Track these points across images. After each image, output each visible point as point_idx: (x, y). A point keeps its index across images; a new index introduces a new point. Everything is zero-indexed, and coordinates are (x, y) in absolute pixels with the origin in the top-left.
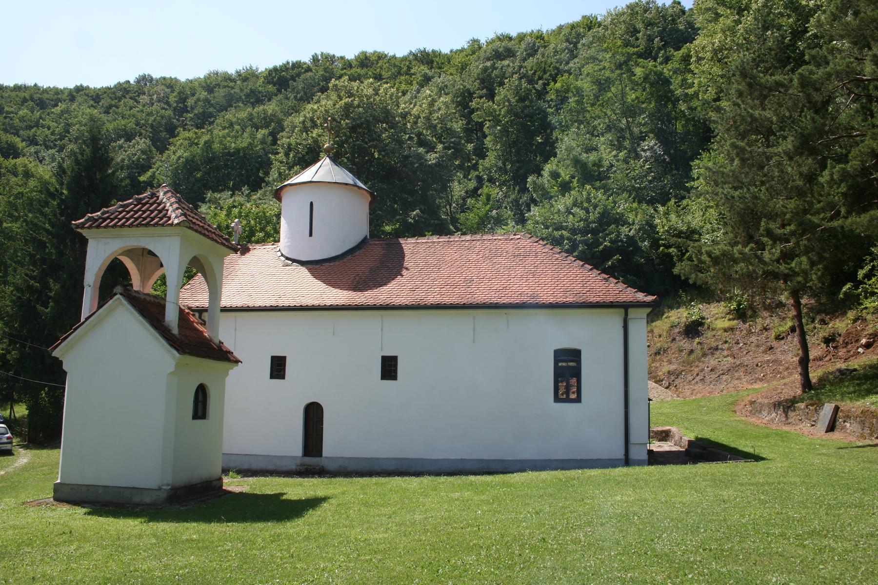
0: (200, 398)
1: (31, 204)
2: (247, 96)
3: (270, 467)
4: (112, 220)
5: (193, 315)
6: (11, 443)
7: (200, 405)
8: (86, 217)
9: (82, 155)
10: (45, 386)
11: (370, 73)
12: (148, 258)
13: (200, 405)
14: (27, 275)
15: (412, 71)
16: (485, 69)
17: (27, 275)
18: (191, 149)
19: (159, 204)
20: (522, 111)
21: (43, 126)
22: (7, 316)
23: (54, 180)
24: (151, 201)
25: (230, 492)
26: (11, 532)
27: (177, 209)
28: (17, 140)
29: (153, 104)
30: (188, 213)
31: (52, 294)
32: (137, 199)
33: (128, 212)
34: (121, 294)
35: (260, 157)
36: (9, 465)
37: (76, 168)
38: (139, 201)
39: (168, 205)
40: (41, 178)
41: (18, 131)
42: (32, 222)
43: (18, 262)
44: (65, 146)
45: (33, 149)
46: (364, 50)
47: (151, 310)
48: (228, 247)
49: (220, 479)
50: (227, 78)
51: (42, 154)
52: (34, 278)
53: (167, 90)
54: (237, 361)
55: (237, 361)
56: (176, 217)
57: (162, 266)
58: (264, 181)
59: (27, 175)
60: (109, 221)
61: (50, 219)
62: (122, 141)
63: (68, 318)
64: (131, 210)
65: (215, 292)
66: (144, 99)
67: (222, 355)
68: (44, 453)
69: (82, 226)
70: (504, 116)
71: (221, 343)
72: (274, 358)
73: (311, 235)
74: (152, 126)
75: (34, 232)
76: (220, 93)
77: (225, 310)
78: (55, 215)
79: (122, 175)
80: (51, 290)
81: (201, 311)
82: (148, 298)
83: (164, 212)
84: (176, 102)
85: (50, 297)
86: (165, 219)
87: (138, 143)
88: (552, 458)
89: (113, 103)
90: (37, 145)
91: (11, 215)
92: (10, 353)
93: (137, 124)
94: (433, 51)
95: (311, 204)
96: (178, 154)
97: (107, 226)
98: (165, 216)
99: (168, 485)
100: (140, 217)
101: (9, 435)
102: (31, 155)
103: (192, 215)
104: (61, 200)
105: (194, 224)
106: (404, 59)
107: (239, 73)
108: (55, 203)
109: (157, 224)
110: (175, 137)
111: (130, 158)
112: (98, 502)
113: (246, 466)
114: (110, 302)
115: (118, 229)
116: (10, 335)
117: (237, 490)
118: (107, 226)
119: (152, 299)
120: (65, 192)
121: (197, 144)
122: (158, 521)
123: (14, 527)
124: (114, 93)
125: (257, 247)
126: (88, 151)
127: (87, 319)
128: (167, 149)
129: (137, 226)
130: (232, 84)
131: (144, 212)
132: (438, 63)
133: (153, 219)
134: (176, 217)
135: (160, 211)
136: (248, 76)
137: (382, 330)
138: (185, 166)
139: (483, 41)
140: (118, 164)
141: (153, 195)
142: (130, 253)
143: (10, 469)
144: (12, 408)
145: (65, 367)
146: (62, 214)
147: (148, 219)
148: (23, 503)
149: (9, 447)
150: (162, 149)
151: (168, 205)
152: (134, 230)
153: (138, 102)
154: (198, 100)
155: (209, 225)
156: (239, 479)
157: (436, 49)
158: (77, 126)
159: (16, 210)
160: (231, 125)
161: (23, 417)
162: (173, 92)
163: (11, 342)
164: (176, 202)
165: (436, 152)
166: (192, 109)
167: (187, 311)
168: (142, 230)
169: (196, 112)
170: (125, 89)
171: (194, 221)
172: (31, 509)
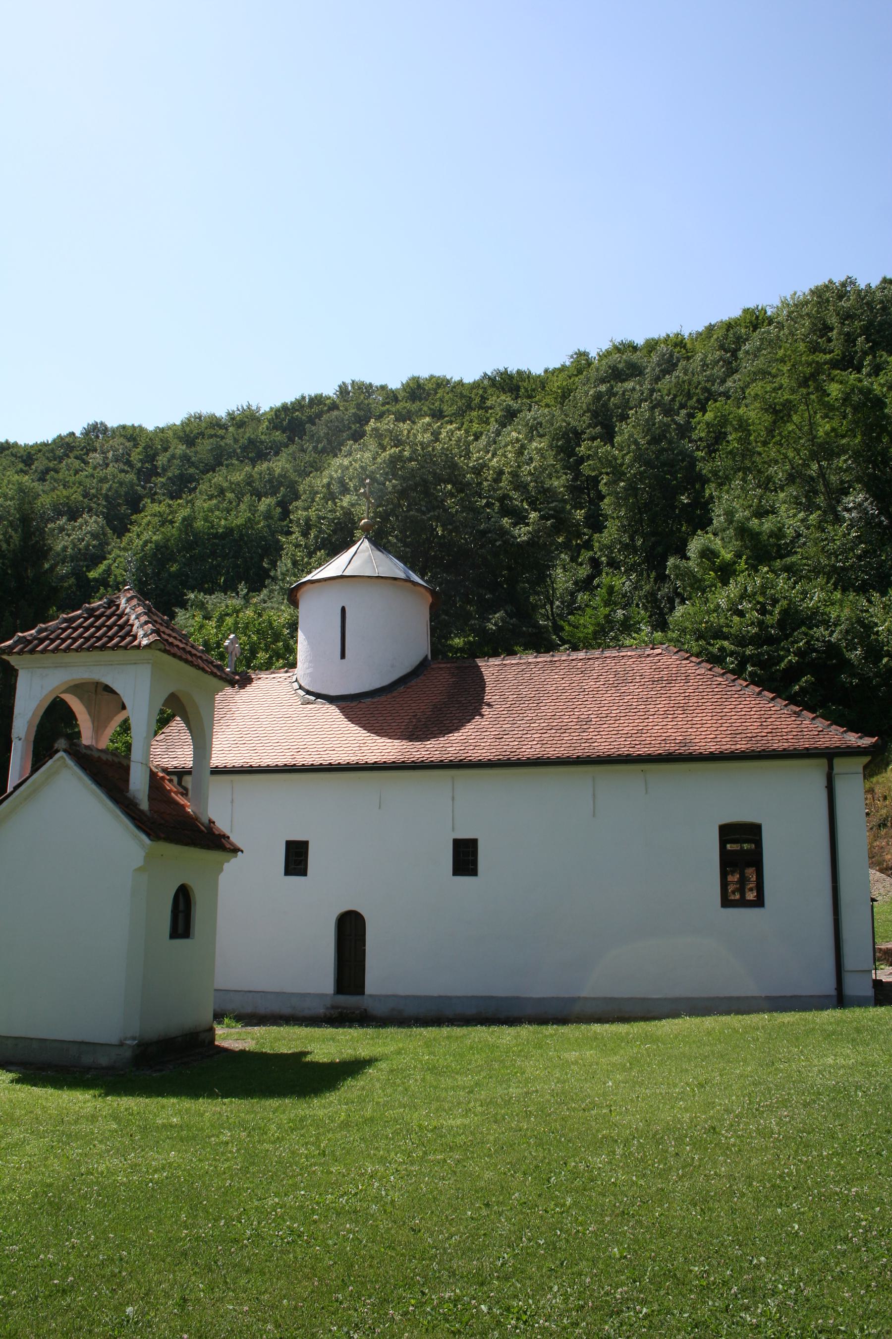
0: (182, 906)
2: (244, 448)
3: (286, 1011)
4: (53, 641)
5: (171, 781)
7: (181, 916)
8: (16, 638)
11: (425, 409)
12: (102, 696)
13: (181, 916)
15: (489, 403)
16: (598, 397)
19: (120, 617)
20: (657, 458)
24: (108, 612)
27: (146, 623)
29: (107, 465)
30: (162, 629)
32: (87, 609)
33: (75, 629)
34: (65, 751)
35: (263, 538)
38: (91, 612)
39: (133, 617)
46: (416, 375)
47: (108, 773)
48: (220, 678)
49: (211, 1030)
50: (214, 423)
53: (128, 444)
54: (235, 850)
55: (235, 850)
56: (145, 635)
57: (124, 707)
58: (269, 577)
64: (80, 626)
66: (95, 458)
67: (214, 842)
69: (9, 650)
70: (631, 466)
71: (211, 822)
72: (289, 844)
73: (343, 656)
74: (106, 497)
76: (204, 446)
81: (181, 774)
82: (104, 757)
83: (127, 628)
84: (141, 460)
86: (129, 639)
88: (721, 995)
89: (51, 465)
93: (86, 495)
94: (519, 372)
95: (343, 610)
98: (128, 634)
99: (134, 1038)
100: (92, 636)
103: (168, 631)
105: (171, 645)
106: (476, 385)
107: (231, 416)
110: (140, 512)
111: (75, 545)
113: (249, 1010)
115: (60, 655)
119: (110, 758)
121: (172, 522)
122: (119, 1095)
124: (52, 451)
126: (16, 537)
127: (16, 788)
128: (129, 531)
129: (88, 649)
130: (221, 432)
131: (98, 629)
132: (526, 390)
133: (111, 639)
134: (145, 635)
135: (121, 627)
136: (244, 420)
137: (232, 802)
138: (155, 554)
139: (593, 354)
142: (78, 689)
147: (105, 639)
150: (121, 530)
151: (133, 617)
152: (84, 654)
153: (86, 463)
154: (173, 457)
155: (193, 646)
156: (238, 1029)
157: (524, 368)
160: (222, 492)
162: (136, 446)
164: (145, 613)
165: (527, 525)
166: (165, 470)
167: (161, 774)
169: (170, 474)
170: (68, 444)
171: (171, 640)
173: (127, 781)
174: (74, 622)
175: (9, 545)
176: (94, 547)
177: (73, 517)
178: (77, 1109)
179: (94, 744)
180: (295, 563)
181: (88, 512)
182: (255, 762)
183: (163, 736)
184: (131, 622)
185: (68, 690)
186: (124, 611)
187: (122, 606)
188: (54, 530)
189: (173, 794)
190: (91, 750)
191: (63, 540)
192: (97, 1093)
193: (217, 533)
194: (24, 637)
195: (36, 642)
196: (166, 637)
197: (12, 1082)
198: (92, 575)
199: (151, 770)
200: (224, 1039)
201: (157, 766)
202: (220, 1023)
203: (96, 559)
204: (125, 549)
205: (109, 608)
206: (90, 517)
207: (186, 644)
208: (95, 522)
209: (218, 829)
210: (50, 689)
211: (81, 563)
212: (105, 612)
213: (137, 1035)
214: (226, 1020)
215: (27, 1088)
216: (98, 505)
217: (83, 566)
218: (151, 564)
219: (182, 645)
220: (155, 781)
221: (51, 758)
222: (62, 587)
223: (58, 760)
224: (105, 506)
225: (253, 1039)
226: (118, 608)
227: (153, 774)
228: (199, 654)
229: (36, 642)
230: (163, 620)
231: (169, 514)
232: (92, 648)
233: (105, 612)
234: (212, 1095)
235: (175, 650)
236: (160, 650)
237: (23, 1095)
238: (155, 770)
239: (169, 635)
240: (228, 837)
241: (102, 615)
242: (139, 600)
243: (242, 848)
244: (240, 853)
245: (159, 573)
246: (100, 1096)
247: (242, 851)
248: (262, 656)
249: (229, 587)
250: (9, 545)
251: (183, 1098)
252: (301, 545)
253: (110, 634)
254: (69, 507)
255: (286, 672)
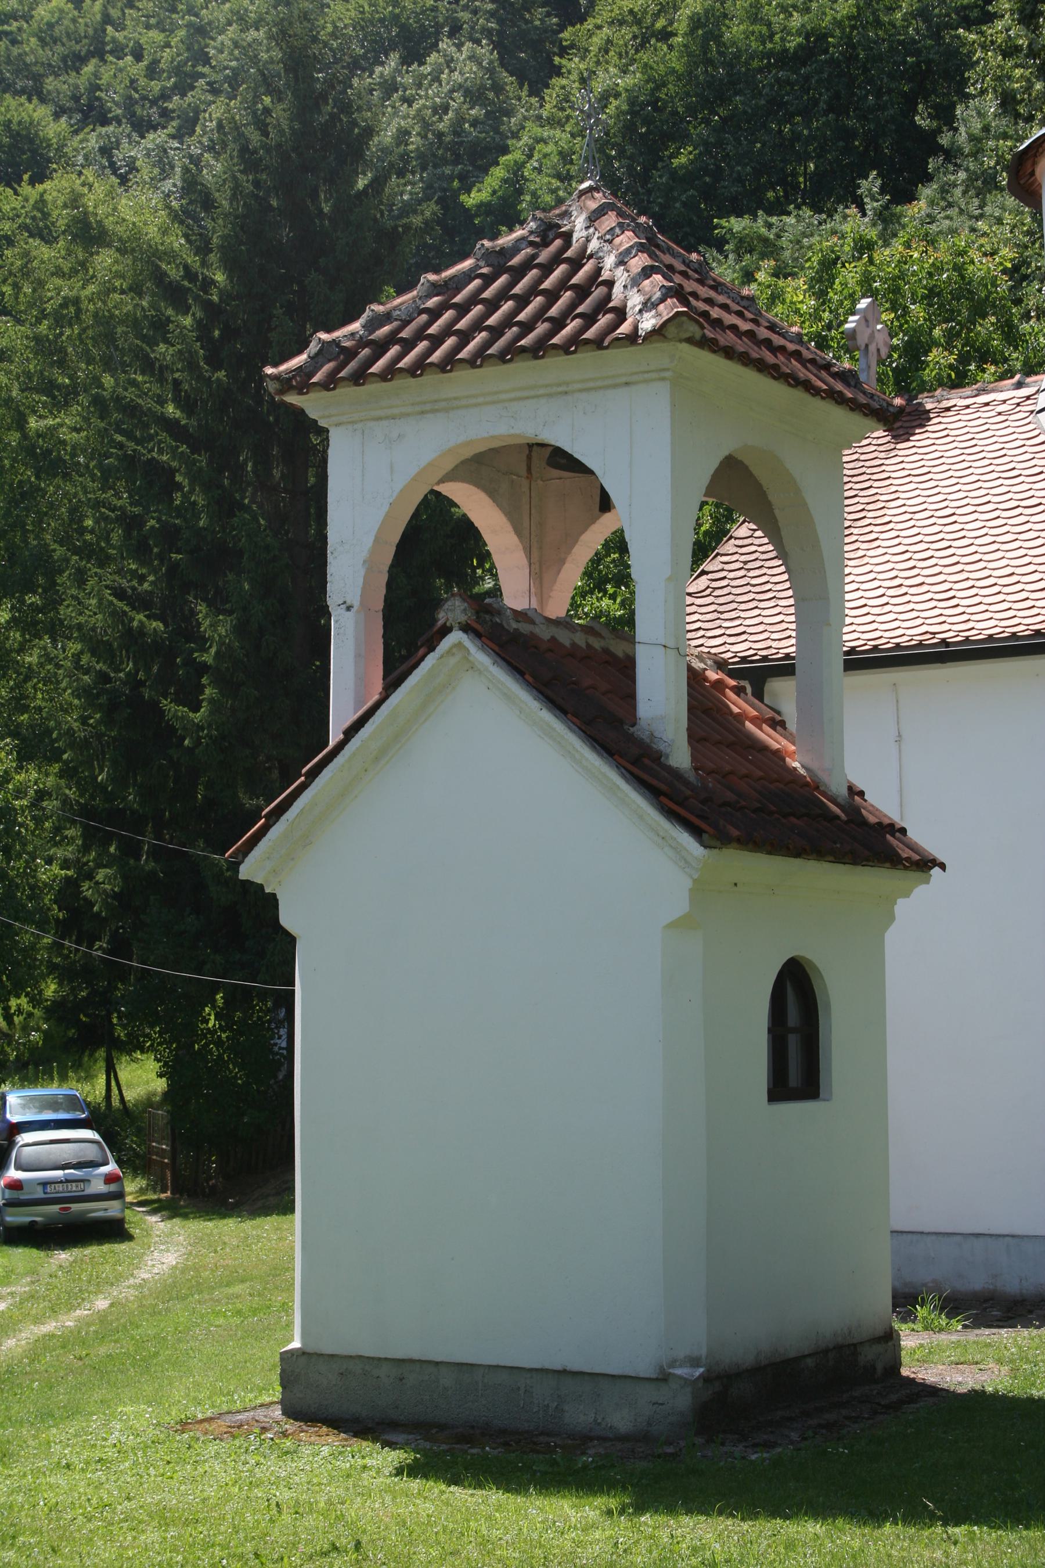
0: (793, 1017)
1: (109, 338)
4: (408, 345)
5: (739, 691)
6: (119, 1195)
7: (793, 1042)
8: (313, 347)
9: (263, 128)
10: (215, 988)
12: (550, 476)
13: (793, 1042)
14: (120, 593)
17: (120, 593)
18: (644, 56)
19: (576, 264)
21: (119, 52)
22: (72, 746)
23: (177, 242)
24: (544, 256)
25: (932, 1391)
26: (151, 1536)
27: (647, 272)
28: (40, 112)
30: (690, 286)
31: (208, 658)
32: (489, 256)
33: (463, 310)
34: (466, 628)
35: (910, 47)
36: (119, 1278)
37: (246, 182)
38: (499, 260)
39: (610, 261)
40: (136, 234)
41: (38, 78)
42: (118, 399)
43: (87, 552)
44: (197, 112)
45: (93, 140)
47: (579, 678)
48: (854, 406)
49: (890, 1337)
51: (126, 151)
52: (141, 602)
54: (925, 864)
55: (925, 864)
56: (648, 305)
57: (605, 504)
58: (936, 149)
59: (88, 234)
60: (394, 350)
61: (176, 383)
62: (393, 61)
63: (281, 736)
64: (474, 300)
65: (816, 592)
67: (869, 843)
68: (230, 1230)
69: (301, 381)
71: (855, 792)
75: (129, 435)
77: (860, 661)
78: (192, 366)
79: (406, 190)
80: (202, 642)
81: (758, 674)
82: (565, 638)
83: (598, 292)
85: (204, 668)
86: (604, 320)
87: (449, 61)
90: (105, 122)
91: (49, 387)
92: (90, 876)
96: (598, 86)
97: (390, 373)
98: (602, 306)
99: (694, 1362)
100: (508, 321)
101: (112, 1167)
102: (88, 162)
103: (704, 292)
104: (207, 306)
105: (718, 330)
108: (187, 321)
109: (575, 342)
110: (582, 20)
111: (426, 125)
112: (442, 1427)
113: (978, 1282)
114: (430, 660)
115: (430, 379)
116: (87, 812)
117: (960, 1380)
118: (390, 373)
119: (580, 639)
120: (220, 277)
121: (665, 35)
122: (671, 1510)
123: (163, 1517)
125: (956, 399)
126: (281, 114)
127: (351, 732)
128: (557, 71)
129: (502, 357)
131: (523, 301)
133: (558, 324)
134: (648, 305)
135: (582, 292)
137: (899, 739)
138: (629, 129)
140: (385, 151)
141: (549, 232)
142: (482, 466)
143: (125, 1291)
144: (111, 1070)
145: (286, 919)
146: (215, 363)
147: (542, 328)
148: (184, 1425)
149: (112, 1209)
150: (538, 74)
151: (610, 261)
152: (490, 372)
155: (772, 327)
156: (956, 1335)
158: (232, 31)
159: (62, 364)
161: (148, 1103)
163: (91, 838)
164: (641, 248)
167: (713, 675)
168: (523, 371)
171: (715, 313)
172: (213, 1448)
173: (630, 696)
174: (458, 290)
175: (266, 134)
176: (474, 123)
177: (414, 55)
178: (568, 1546)
179: (534, 605)
180: (1008, 102)
181: (451, 35)
182: (953, 628)
183: (703, 582)
184: (605, 275)
185: (450, 477)
186: (584, 248)
187: (579, 235)
188: (371, 91)
189: (748, 724)
190: (532, 622)
191: (395, 114)
192: (613, 1503)
193: (786, 50)
194: (335, 343)
195: (366, 351)
196: (702, 306)
197: (399, 1472)
198: (472, 199)
199: (690, 669)
200: (923, 1361)
201: (700, 657)
202: (908, 1317)
203: (481, 155)
204: (553, 122)
205: (546, 244)
206: (459, 46)
207: (755, 321)
208: (472, 58)
209: (875, 811)
210: (413, 471)
211: (447, 170)
212: (534, 257)
213: (704, 1352)
214: (921, 1312)
215: (436, 1488)
216: (475, 12)
217: (451, 178)
218: (621, 153)
219: (745, 326)
220: (702, 697)
221: (432, 649)
222: (407, 228)
223: (449, 652)
224: (492, 14)
225: (1000, 1361)
226: (568, 244)
227: (695, 677)
228: (791, 347)
229: (366, 351)
230: (687, 263)
231: (656, 16)
232: (511, 353)
233: (534, 257)
234: (914, 1515)
235: (727, 339)
236: (690, 341)
237: (429, 1507)
238: (698, 665)
239: (709, 301)
240: (903, 831)
241: (527, 265)
242: (620, 214)
243: (941, 857)
244: (936, 871)
245: (645, 177)
246: (622, 1512)
247: (943, 866)
248: (938, 358)
249: (830, 192)
250: (266, 134)
251: (840, 1522)
252: (1018, 49)
253: (553, 312)
254: (404, 28)
255: (1019, 385)
